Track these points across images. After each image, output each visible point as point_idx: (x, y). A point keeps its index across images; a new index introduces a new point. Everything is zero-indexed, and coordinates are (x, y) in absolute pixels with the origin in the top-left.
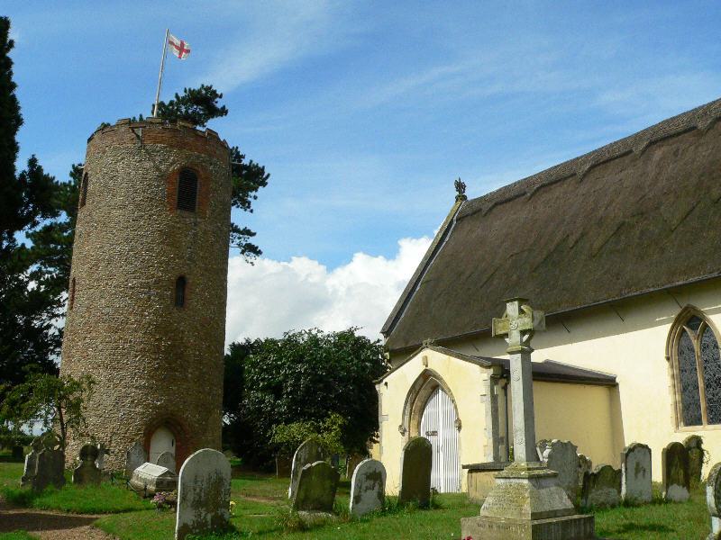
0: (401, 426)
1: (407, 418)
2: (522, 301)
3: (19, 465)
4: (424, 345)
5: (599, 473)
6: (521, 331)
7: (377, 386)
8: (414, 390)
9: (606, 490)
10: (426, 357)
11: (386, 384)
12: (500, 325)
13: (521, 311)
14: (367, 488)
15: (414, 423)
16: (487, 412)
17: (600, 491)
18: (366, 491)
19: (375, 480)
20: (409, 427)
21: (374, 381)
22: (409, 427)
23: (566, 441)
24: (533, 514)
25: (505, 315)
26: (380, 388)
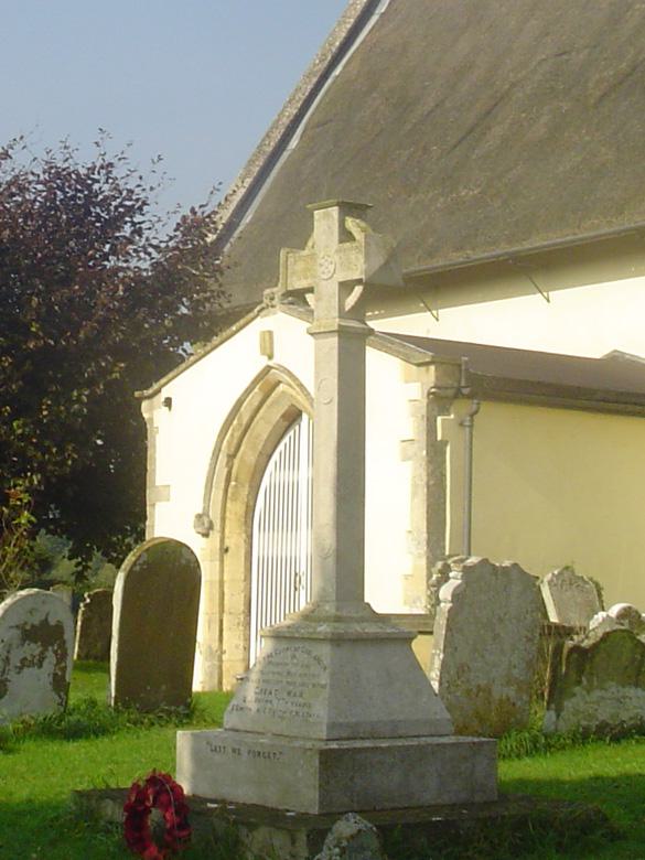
0: (199, 517)
1: (217, 494)
2: (348, 209)
3: (96, 677)
4: (266, 301)
5: (595, 646)
6: (342, 284)
7: (144, 404)
8: (237, 424)
9: (613, 689)
10: (270, 333)
11: (168, 402)
12: (300, 266)
13: (346, 236)
14: (24, 663)
15: (236, 509)
16: (415, 486)
17: (597, 693)
18: (21, 669)
19: (46, 645)
20: (223, 519)
21: (137, 394)
22: (223, 519)
23: (507, 563)
24: (332, 726)
25: (310, 244)
26: (153, 412)
